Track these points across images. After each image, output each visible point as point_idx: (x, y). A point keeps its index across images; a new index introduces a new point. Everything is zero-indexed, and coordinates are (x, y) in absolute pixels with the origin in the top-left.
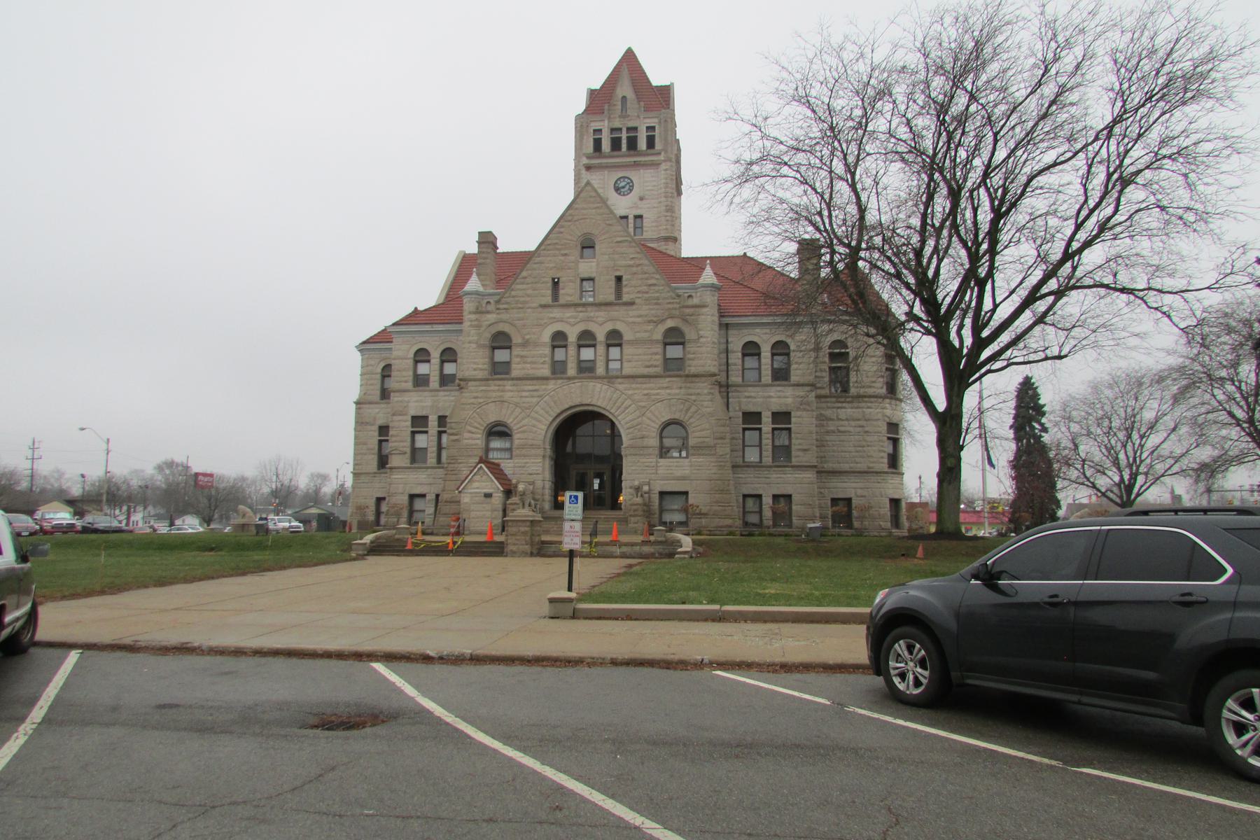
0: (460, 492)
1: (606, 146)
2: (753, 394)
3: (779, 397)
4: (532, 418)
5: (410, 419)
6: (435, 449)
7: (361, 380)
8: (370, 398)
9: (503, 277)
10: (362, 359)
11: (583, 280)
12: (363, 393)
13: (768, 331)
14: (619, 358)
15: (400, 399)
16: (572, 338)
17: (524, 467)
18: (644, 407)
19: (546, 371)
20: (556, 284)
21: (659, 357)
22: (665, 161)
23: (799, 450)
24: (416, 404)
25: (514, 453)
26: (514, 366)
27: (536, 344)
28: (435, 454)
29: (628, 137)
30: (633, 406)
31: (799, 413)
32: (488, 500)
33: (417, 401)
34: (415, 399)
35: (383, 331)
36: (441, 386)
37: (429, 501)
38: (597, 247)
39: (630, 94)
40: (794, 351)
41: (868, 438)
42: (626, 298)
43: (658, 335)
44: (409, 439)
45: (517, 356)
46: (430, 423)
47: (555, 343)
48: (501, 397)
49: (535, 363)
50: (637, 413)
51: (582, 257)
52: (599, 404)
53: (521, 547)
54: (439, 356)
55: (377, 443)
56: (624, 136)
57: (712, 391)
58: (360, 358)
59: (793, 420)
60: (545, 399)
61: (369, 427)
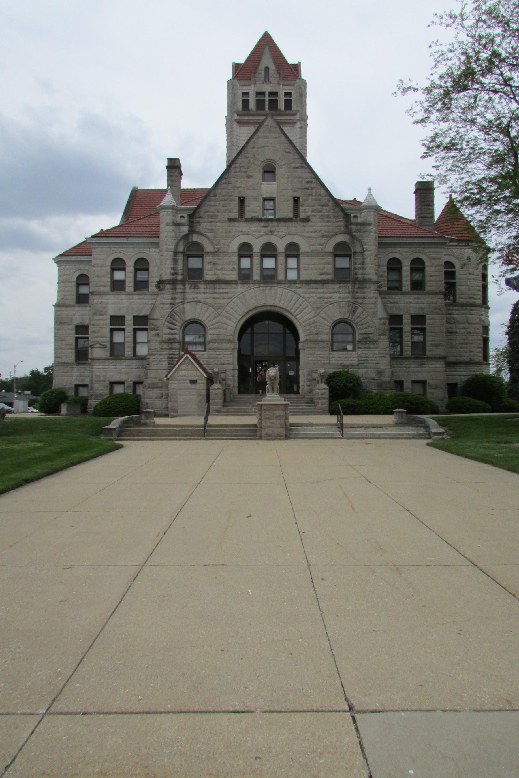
0: (168, 379)
1: (252, 105)
2: (395, 300)
3: (417, 303)
4: (223, 316)
5: (109, 317)
6: (132, 344)
7: (58, 288)
8: (67, 302)
9: (191, 199)
10: (59, 270)
11: (265, 199)
12: (60, 298)
13: (408, 250)
14: (296, 267)
15: (100, 301)
16: (257, 248)
17: (216, 358)
18: (319, 308)
19: (234, 276)
20: (242, 201)
21: (330, 266)
22: (299, 120)
23: (432, 345)
24: (114, 305)
25: (208, 346)
26: (206, 272)
27: (226, 253)
28: (131, 348)
29: (269, 100)
30: (310, 307)
31: (432, 316)
32: (193, 386)
33: (114, 303)
34: (112, 301)
35: (84, 242)
36: (135, 291)
37: (128, 387)
38: (277, 172)
39: (272, 68)
40: (428, 266)
41: (470, 337)
42: (302, 215)
43: (330, 248)
44: (108, 335)
45: (209, 263)
46: (126, 321)
47: (242, 253)
48: (195, 298)
49: (225, 270)
50: (313, 313)
51: (264, 180)
52: (281, 305)
53: (276, 429)
54: (133, 265)
55: (74, 339)
56: (267, 98)
57: (375, 296)
58: (57, 268)
59: (427, 321)
60: (234, 300)
61: (67, 327)
